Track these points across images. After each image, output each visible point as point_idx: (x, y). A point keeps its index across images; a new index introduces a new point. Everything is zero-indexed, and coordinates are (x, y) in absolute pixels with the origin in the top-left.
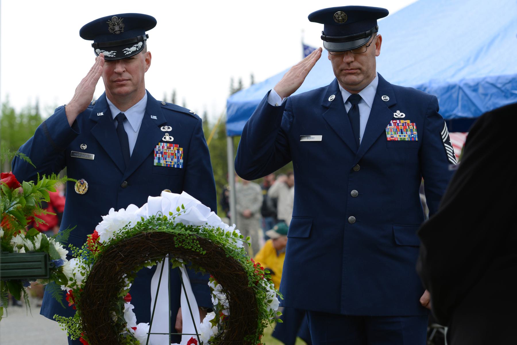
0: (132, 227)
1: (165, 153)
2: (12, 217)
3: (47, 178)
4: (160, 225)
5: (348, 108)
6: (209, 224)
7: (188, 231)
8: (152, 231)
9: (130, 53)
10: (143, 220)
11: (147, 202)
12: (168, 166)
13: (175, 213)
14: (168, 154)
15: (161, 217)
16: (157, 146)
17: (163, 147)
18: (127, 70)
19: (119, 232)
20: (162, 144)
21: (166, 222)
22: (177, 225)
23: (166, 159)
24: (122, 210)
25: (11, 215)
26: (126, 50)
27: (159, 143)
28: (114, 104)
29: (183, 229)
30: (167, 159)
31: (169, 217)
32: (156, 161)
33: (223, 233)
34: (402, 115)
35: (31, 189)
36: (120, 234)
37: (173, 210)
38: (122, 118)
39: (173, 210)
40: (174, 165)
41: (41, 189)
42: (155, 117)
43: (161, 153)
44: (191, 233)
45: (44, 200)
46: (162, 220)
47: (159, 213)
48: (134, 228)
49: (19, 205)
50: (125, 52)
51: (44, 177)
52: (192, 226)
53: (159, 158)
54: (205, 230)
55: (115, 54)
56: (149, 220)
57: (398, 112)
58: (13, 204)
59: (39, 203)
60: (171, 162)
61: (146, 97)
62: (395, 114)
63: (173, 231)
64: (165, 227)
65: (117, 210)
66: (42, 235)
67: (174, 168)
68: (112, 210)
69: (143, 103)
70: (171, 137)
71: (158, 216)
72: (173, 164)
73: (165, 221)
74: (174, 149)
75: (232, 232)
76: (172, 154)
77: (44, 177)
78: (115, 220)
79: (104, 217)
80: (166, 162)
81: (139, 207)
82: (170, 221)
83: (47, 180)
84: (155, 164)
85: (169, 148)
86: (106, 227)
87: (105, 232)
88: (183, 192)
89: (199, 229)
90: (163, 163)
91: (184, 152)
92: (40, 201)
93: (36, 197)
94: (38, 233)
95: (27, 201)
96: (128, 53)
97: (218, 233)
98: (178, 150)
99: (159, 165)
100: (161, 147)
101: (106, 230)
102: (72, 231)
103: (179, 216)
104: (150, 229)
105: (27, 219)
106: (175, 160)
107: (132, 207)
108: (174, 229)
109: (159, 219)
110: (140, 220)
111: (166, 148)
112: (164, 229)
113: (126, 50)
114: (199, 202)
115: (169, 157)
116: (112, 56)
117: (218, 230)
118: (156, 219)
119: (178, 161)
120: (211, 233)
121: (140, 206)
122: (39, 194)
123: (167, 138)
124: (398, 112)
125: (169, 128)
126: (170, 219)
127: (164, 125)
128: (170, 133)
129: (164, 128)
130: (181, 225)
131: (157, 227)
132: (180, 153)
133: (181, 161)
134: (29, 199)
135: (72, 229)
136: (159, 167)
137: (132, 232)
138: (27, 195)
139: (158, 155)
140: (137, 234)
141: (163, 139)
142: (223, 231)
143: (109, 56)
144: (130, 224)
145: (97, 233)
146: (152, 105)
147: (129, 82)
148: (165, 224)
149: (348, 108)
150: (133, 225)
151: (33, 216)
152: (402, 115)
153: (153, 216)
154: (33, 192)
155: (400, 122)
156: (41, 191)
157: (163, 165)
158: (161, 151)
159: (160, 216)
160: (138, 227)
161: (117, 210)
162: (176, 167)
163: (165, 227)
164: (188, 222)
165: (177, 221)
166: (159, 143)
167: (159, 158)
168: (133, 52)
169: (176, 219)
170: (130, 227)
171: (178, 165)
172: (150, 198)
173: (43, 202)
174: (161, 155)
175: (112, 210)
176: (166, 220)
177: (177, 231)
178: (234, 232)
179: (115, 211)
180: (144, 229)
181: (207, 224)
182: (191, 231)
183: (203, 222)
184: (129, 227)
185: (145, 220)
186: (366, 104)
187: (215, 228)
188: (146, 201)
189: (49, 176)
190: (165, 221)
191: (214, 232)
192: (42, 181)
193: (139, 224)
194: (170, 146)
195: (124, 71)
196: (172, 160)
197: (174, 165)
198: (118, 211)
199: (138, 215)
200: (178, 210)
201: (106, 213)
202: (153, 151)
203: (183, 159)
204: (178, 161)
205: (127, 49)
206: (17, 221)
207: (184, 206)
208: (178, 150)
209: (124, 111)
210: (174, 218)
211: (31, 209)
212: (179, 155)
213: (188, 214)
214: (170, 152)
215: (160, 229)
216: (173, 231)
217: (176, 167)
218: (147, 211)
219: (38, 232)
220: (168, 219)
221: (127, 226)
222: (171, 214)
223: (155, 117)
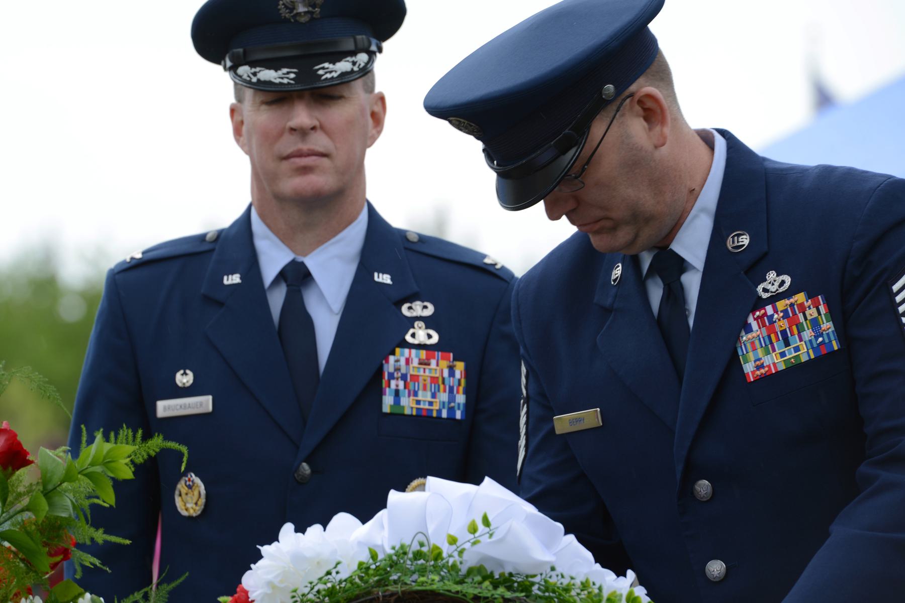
0: (344, 575)
1: (415, 378)
2: (9, 549)
3: (107, 439)
4: (422, 571)
5: (277, 300)
6: (559, 570)
7: (501, 590)
8: (398, 588)
9: (335, 75)
10: (374, 556)
11: (384, 506)
12: (424, 413)
13: (464, 537)
14: (423, 378)
15: (425, 549)
16: (392, 359)
17: (408, 361)
18: (322, 128)
19: (306, 590)
20: (406, 351)
21: (440, 563)
22: (470, 571)
23: (416, 394)
24: (315, 530)
25: (7, 544)
26: (323, 68)
27: (398, 350)
28: (276, 233)
29: (487, 583)
30: (420, 393)
31: (446, 549)
32: (388, 401)
33: (600, 594)
34: (783, 282)
35: (61, 472)
36: (311, 596)
37: (458, 528)
38: (297, 277)
39: (458, 528)
40: (439, 411)
41: (91, 469)
42: (386, 279)
43: (404, 377)
44: (508, 595)
45: (96, 501)
46: (427, 557)
47: (421, 538)
48: (350, 580)
49: (27, 515)
50: (321, 72)
51: (99, 436)
52: (511, 574)
53: (397, 393)
54: (547, 587)
55: (292, 76)
56: (390, 557)
57: (772, 275)
58: (12, 511)
59: (82, 510)
60: (431, 403)
61: (364, 216)
62: (760, 289)
63: (458, 588)
64: (437, 578)
65: (301, 528)
66: (92, 599)
67: (439, 417)
68: (288, 529)
69: (357, 230)
70: (432, 332)
71: (415, 547)
72: (436, 407)
73: (436, 559)
74: (439, 366)
75: (625, 593)
76: (434, 380)
77: (99, 436)
78: (298, 558)
79: (265, 550)
80: (418, 402)
81: (364, 519)
82: (451, 561)
83: (108, 446)
84: (386, 409)
85: (424, 363)
86: (270, 577)
87: (269, 592)
88: (487, 480)
89: (533, 584)
90: (408, 405)
91: (467, 373)
92: (86, 503)
93: (75, 492)
94: (81, 595)
95: (51, 504)
96: (328, 76)
97: (584, 594)
98: (451, 369)
99: (397, 411)
100: (403, 362)
101: (270, 584)
102: (175, 589)
103: (477, 548)
104: (395, 582)
105: (51, 555)
106: (444, 397)
107: (343, 521)
108: (461, 582)
109: (418, 555)
110: (365, 557)
111: (415, 362)
112: (434, 582)
113: (323, 68)
114: (530, 509)
115: (425, 388)
116: (285, 81)
117: (585, 585)
118: (411, 555)
119: (452, 399)
120: (567, 596)
121: (364, 518)
122: (85, 485)
123: (421, 335)
124: (772, 275)
125: (425, 307)
126: (450, 556)
127: (411, 298)
128: (429, 322)
129: (410, 308)
130: (481, 572)
131: (415, 577)
132: (458, 375)
133: (461, 398)
134: (56, 499)
135: (173, 585)
136: (397, 416)
137: (345, 590)
138: (50, 487)
139: (393, 383)
140: (357, 597)
141: (408, 338)
142: (600, 589)
143: (278, 81)
144: (339, 568)
145: (246, 592)
146: (382, 242)
147: (325, 161)
148: (436, 569)
149: (277, 300)
150: (347, 570)
151: (65, 546)
152: (783, 282)
153: (402, 547)
154: (68, 477)
155: (776, 311)
156: (89, 476)
157: (407, 412)
158: (403, 371)
159: (422, 545)
160: (361, 578)
161: (301, 528)
162: (444, 414)
163: (437, 578)
164: (500, 563)
165: (470, 560)
166: (398, 350)
167: (397, 393)
168: (343, 74)
169: (466, 556)
170: (339, 577)
171: (451, 410)
172: (394, 496)
173: (94, 507)
174: (401, 384)
175: (288, 529)
176: (438, 556)
177: (470, 590)
178: (630, 594)
179: (296, 531)
180: (379, 583)
181: (553, 569)
182: (509, 588)
183: (542, 564)
184: (335, 578)
185: (381, 556)
186: (694, 268)
187: (578, 582)
188: (383, 505)
189: (112, 435)
190: (436, 559)
191: (573, 593)
192: (93, 447)
193: (363, 568)
194: (428, 358)
195: (313, 128)
196: (434, 396)
197: (439, 411)
198: (303, 532)
199: (360, 543)
200: (473, 529)
201: (272, 537)
202: (380, 372)
203: (467, 392)
204: (452, 399)
205: (326, 65)
206: (23, 560)
207: (490, 518)
208: (451, 369)
209: (305, 255)
210: (461, 553)
211: (60, 527)
212: (452, 382)
213: (501, 541)
214: (425, 374)
215: (423, 583)
216: (458, 588)
217: (444, 414)
218: (386, 533)
219: (82, 590)
220: (444, 555)
221: (329, 573)
222: (453, 541)
223: (386, 279)
